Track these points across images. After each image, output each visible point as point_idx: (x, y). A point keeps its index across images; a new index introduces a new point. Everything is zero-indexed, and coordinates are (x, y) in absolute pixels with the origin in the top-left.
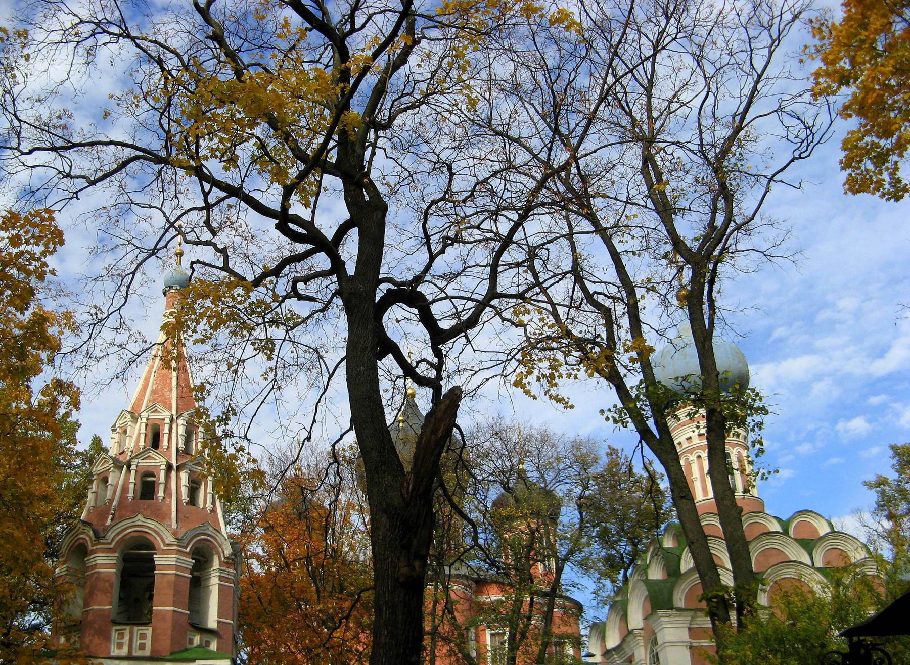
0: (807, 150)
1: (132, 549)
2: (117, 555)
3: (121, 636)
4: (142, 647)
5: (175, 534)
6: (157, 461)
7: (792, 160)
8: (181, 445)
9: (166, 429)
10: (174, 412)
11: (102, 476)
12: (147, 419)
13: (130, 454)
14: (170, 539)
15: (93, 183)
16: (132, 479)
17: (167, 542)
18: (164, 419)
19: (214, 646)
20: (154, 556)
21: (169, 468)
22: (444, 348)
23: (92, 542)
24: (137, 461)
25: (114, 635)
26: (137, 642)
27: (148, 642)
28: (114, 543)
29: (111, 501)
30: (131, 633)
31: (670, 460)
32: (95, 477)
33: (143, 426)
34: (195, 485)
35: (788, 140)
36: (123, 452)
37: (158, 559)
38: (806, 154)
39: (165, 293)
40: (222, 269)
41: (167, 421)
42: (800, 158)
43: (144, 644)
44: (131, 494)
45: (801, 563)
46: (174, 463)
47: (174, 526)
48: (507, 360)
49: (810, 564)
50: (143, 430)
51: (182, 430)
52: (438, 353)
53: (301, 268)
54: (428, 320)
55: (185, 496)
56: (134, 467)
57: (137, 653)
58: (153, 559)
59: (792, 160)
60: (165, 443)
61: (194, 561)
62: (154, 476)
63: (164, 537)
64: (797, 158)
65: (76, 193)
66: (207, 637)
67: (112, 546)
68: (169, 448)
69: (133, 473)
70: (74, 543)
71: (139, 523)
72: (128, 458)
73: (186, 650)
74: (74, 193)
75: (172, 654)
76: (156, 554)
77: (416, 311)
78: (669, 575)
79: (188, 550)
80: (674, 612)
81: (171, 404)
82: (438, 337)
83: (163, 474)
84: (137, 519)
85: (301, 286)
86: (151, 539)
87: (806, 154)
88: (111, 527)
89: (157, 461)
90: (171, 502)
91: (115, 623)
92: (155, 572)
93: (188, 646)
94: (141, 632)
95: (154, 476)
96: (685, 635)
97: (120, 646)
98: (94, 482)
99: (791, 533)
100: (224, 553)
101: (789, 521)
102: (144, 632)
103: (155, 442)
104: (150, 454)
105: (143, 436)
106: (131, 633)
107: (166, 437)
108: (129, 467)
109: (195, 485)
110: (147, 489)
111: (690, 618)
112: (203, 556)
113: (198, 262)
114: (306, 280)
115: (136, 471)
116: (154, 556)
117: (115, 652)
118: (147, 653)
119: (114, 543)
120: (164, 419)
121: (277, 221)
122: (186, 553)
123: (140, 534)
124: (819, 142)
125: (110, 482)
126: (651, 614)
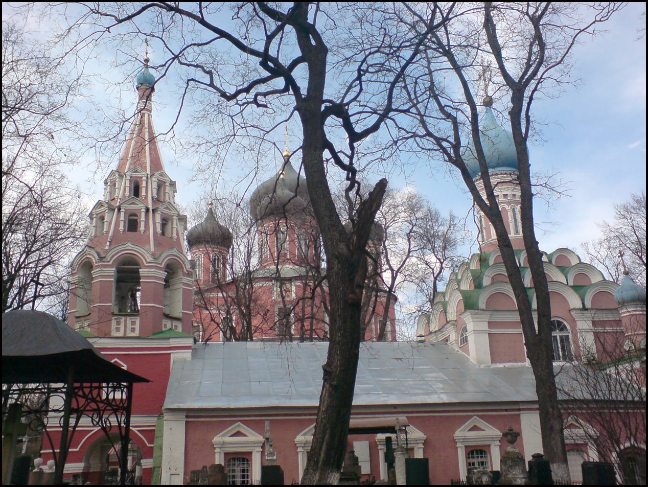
0: (607, 15)
1: (124, 265)
2: (114, 269)
3: (118, 323)
4: (133, 330)
5: (153, 255)
6: (139, 206)
7: (594, 23)
8: (155, 195)
9: (144, 184)
10: (148, 172)
11: (100, 215)
12: (131, 177)
13: (119, 200)
14: (150, 259)
15: (120, 21)
16: (122, 218)
17: (148, 260)
18: (142, 177)
19: (180, 329)
20: (140, 270)
21: (147, 210)
22: (355, 144)
23: (96, 261)
24: (125, 205)
25: (114, 323)
26: (129, 326)
27: (137, 326)
28: (111, 262)
29: (108, 232)
30: (125, 321)
31: (497, 221)
32: (95, 216)
33: (128, 183)
34: (164, 222)
35: (594, 8)
36: (114, 199)
37: (143, 272)
38: (606, 18)
39: (137, 88)
40: (209, 85)
41: (144, 178)
42: (600, 21)
43: (134, 328)
44: (121, 228)
45: (561, 283)
46: (150, 207)
47: (152, 248)
48: (385, 148)
49: (566, 283)
50: (128, 184)
51: (155, 185)
52: (352, 148)
53: (262, 88)
54: (348, 126)
55: (159, 230)
56: (122, 210)
57: (130, 334)
58: (139, 271)
59: (594, 23)
60: (143, 193)
61: (166, 273)
62: (136, 216)
63: (146, 258)
64: (598, 21)
65: (108, 28)
66: (175, 323)
67: (110, 263)
68: (146, 197)
69: (122, 215)
70: (81, 262)
71: (129, 248)
72: (118, 204)
73: (162, 332)
74: (107, 28)
75: (154, 334)
76: (141, 268)
77: (341, 120)
78: (476, 287)
79: (162, 266)
80: (479, 311)
81: (146, 167)
82: (354, 137)
83: (143, 215)
84: (127, 245)
85: (259, 98)
86: (139, 260)
87: (606, 18)
88: (110, 250)
89: (139, 206)
90: (149, 233)
91: (113, 314)
92: (141, 280)
93: (164, 329)
94: (133, 320)
95: (136, 216)
96: (485, 326)
97: (118, 330)
98: (94, 219)
99: (554, 262)
100: (186, 267)
101: (552, 254)
102: (134, 320)
103: (136, 191)
104: (135, 202)
105: (127, 189)
106: (125, 321)
107: (144, 190)
108: (119, 209)
109: (164, 222)
110: (133, 225)
111: (489, 316)
112: (170, 269)
113: (192, 80)
114: (265, 95)
115: (125, 213)
116: (140, 270)
117: (114, 334)
118: (137, 334)
119: (111, 262)
120: (142, 177)
121: (261, 59)
122: (161, 268)
123: (129, 255)
124: (616, 10)
125: (106, 220)
126: (464, 312)
